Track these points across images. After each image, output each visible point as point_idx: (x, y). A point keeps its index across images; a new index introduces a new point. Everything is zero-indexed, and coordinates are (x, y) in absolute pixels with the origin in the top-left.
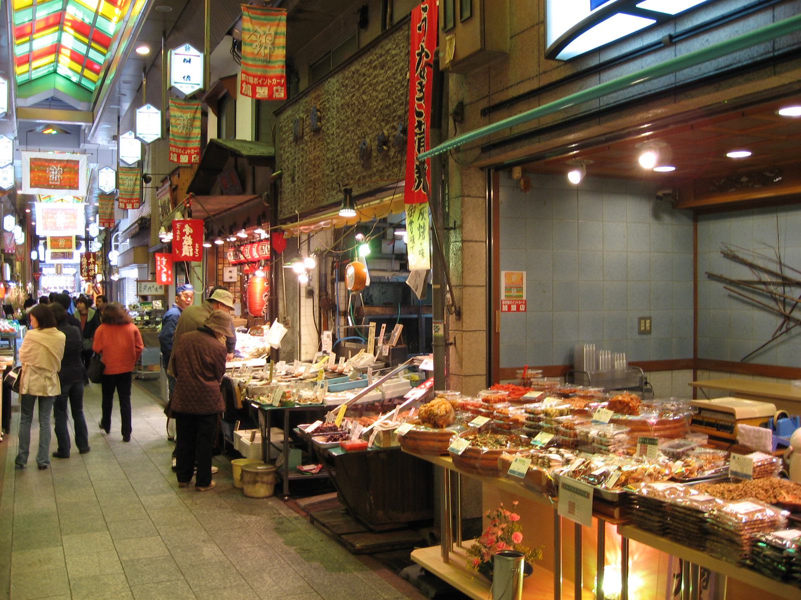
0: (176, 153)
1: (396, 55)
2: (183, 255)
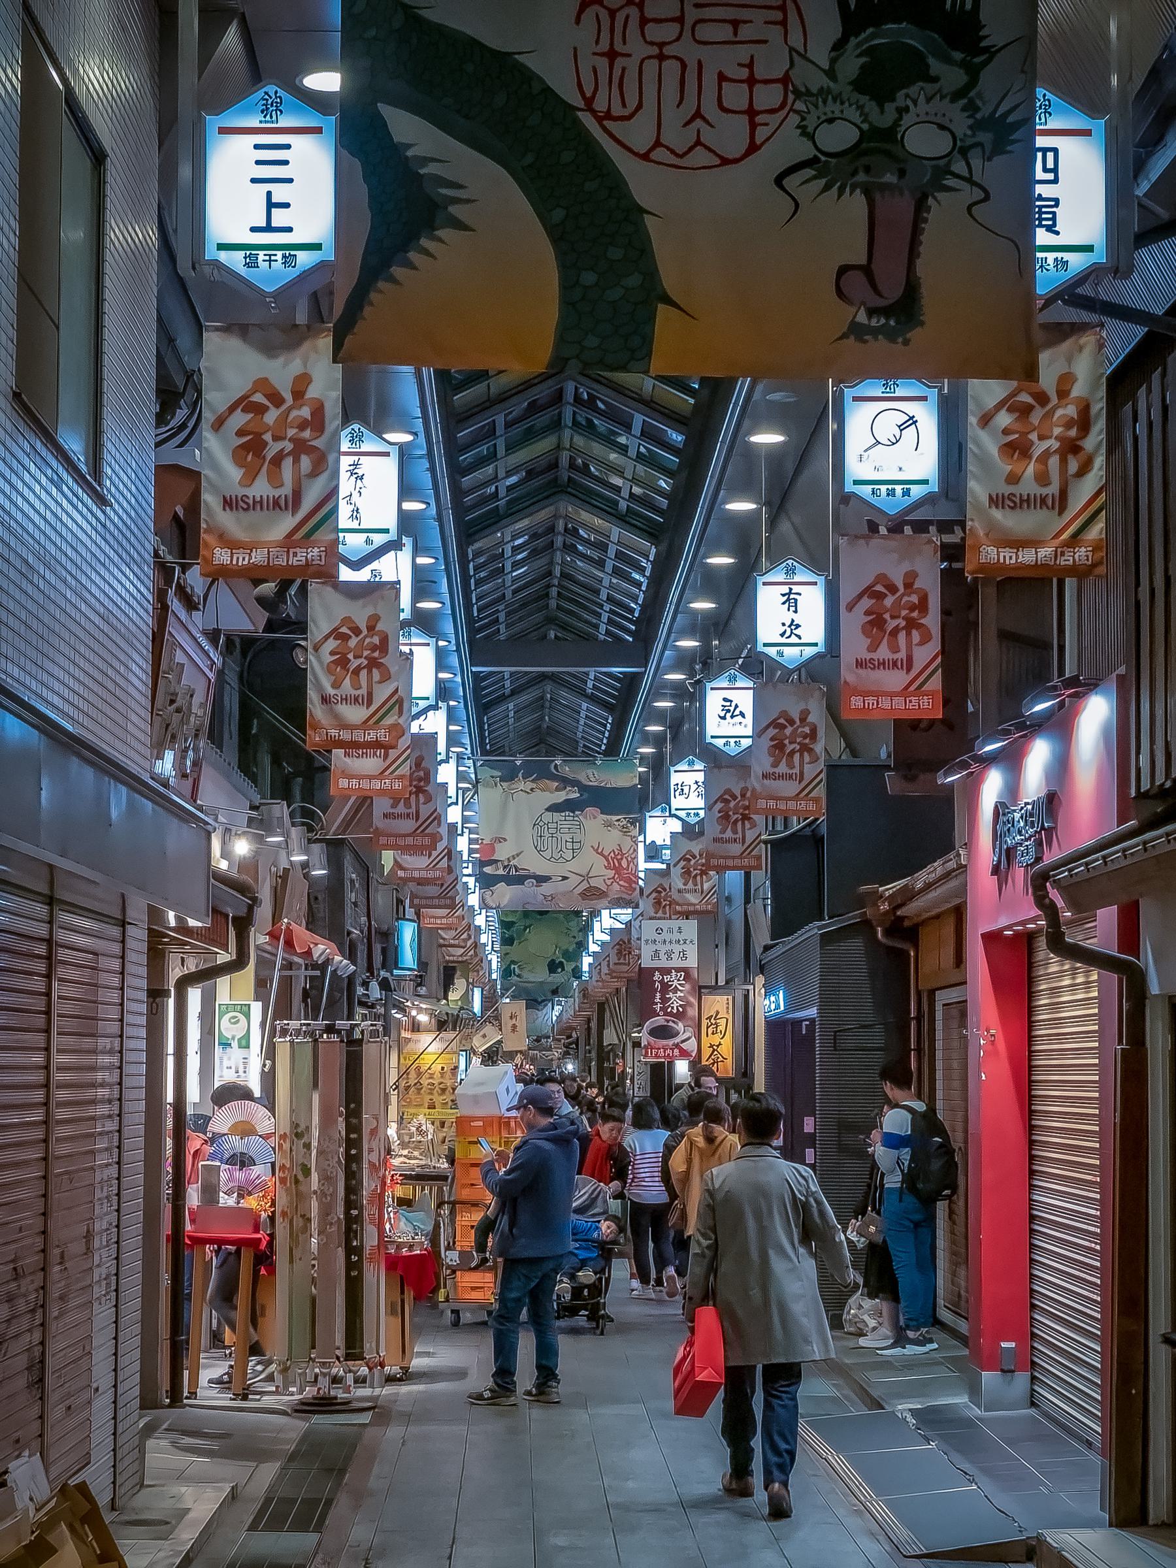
1: (271, 117)
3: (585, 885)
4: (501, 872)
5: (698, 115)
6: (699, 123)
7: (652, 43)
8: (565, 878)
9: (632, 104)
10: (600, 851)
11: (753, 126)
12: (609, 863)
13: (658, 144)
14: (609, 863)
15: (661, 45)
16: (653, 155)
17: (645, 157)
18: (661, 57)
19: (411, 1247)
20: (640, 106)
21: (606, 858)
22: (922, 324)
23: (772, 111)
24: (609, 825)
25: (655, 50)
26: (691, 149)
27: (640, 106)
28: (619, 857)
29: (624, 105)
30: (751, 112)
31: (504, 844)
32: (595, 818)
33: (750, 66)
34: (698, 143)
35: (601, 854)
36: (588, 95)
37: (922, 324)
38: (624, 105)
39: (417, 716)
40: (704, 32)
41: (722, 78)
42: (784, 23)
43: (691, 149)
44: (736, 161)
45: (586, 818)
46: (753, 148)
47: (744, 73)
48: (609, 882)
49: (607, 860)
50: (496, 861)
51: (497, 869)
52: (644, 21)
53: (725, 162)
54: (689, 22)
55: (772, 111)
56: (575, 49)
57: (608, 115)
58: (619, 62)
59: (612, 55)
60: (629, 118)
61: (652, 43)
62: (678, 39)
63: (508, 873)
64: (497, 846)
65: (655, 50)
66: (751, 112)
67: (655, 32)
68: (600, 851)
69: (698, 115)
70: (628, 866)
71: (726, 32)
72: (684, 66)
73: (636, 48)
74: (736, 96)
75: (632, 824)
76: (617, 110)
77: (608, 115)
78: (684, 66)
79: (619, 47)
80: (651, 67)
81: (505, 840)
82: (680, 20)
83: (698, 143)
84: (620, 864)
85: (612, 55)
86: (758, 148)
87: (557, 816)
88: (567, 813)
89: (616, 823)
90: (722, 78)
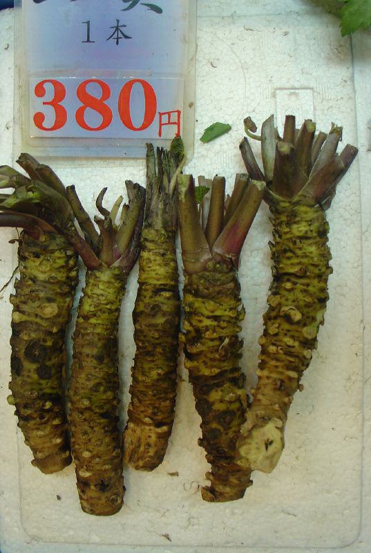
0: (262, 14)
19: (213, 347)
22: (73, 187)
37: (73, 187)
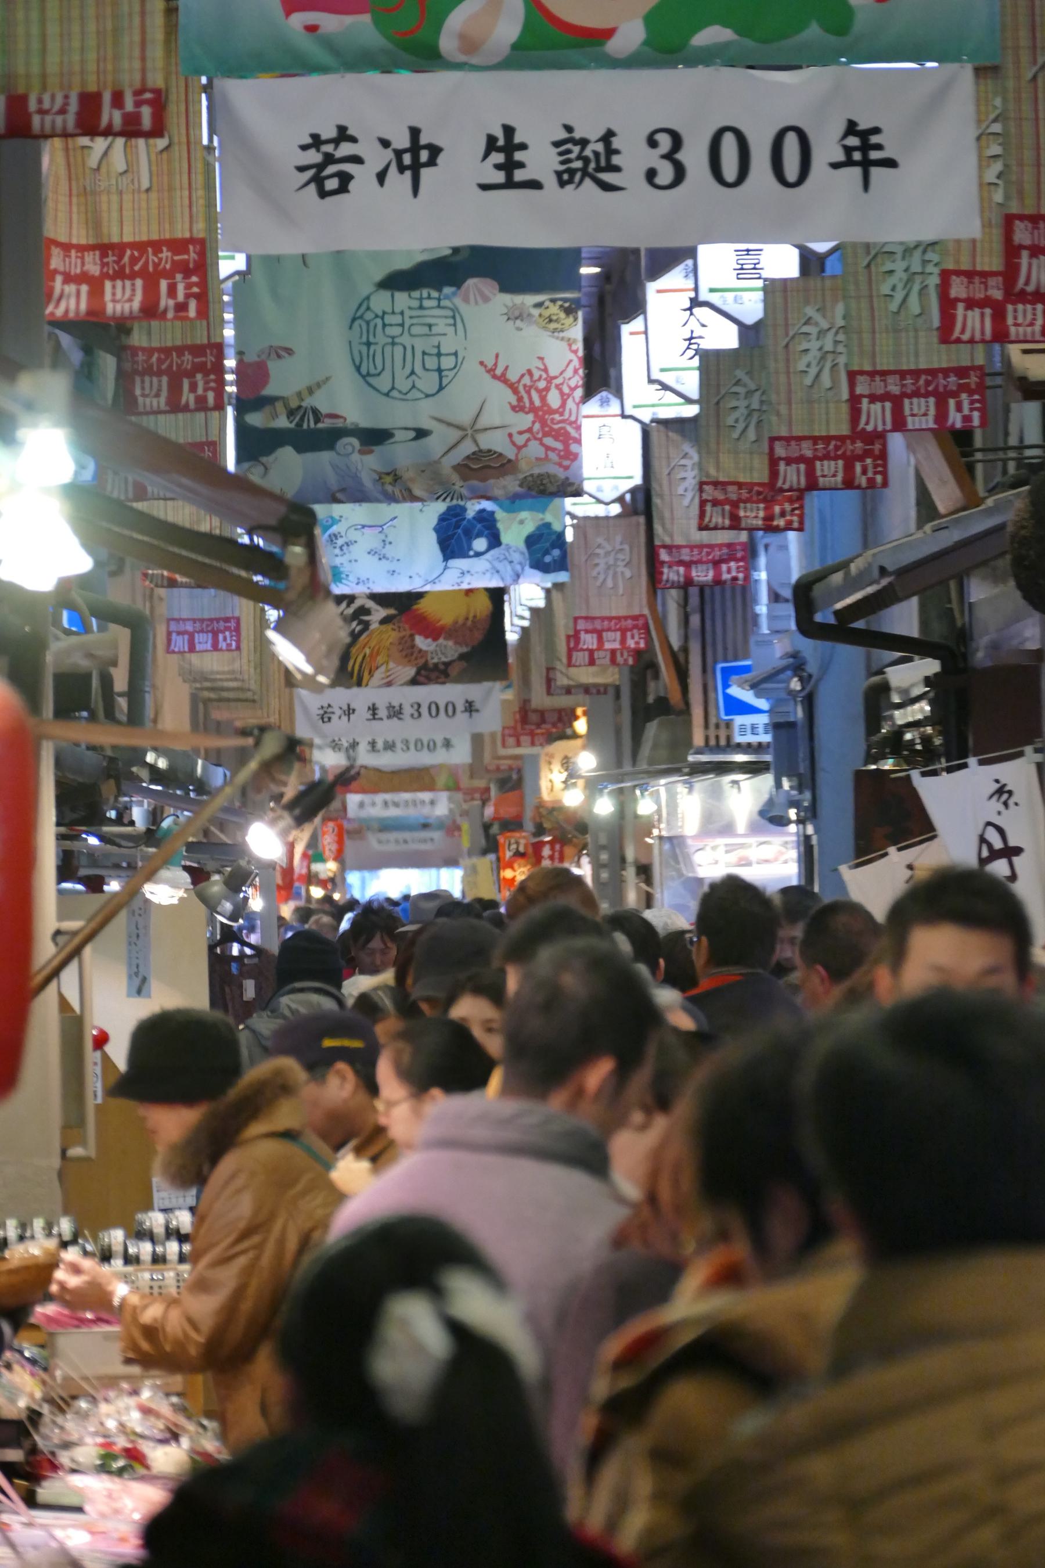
0: (899, 706)
2: (936, 426)
3: (467, 448)
4: (282, 422)
5: (413, 373)
6: (414, 377)
7: (388, 336)
8: (421, 434)
9: (380, 368)
10: (498, 372)
11: (441, 378)
12: (520, 399)
13: (393, 388)
14: (520, 399)
15: (393, 338)
16: (391, 394)
17: (387, 395)
18: (393, 344)
20: (383, 369)
21: (513, 388)
22: (348, 191)
23: (451, 369)
24: (517, 316)
25: (390, 340)
26: (410, 390)
27: (383, 369)
28: (542, 384)
29: (376, 368)
30: (439, 355)
31: (288, 361)
32: (486, 299)
33: (438, 347)
34: (414, 386)
35: (503, 379)
36: (357, 363)
37: (348, 191)
38: (376, 368)
39: (382, 937)
40: (415, 330)
41: (424, 353)
42: (455, 325)
43: (410, 390)
44: (433, 395)
45: (466, 300)
46: (441, 388)
47: (435, 351)
48: (520, 440)
49: (515, 391)
50: (271, 400)
51: (275, 416)
52: (384, 325)
53: (427, 396)
54: (406, 326)
55: (451, 369)
56: (350, 342)
57: (368, 374)
58: (372, 348)
59: (368, 344)
60: (379, 374)
61: (388, 336)
62: (401, 335)
63: (299, 425)
64: (273, 366)
65: (390, 340)
66: (439, 370)
67: (390, 331)
68: (498, 372)
69: (413, 373)
70: (563, 404)
71: (426, 330)
72: (405, 348)
73: (381, 339)
74: (431, 363)
75: (568, 311)
76: (372, 371)
77: (368, 374)
78: (405, 348)
79: (372, 339)
80: (388, 349)
81: (289, 351)
82: (402, 325)
83: (414, 386)
84: (543, 399)
85: (368, 344)
86: (444, 388)
87: (402, 299)
88: (425, 293)
89: (536, 312)
90: (424, 353)
